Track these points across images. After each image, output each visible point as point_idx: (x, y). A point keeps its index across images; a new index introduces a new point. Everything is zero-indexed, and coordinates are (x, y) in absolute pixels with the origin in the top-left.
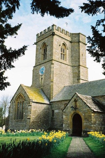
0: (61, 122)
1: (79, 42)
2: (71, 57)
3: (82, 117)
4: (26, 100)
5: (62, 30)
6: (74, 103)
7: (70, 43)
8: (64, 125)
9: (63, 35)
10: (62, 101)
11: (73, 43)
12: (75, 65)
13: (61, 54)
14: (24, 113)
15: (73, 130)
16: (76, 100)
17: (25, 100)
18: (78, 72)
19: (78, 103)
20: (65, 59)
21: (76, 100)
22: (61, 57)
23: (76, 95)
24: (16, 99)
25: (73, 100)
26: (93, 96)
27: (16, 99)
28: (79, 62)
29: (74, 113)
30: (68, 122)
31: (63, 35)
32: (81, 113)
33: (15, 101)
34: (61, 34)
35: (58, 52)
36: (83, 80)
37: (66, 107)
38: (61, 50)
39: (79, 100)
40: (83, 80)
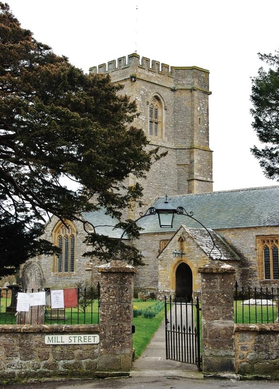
0: (151, 277)
1: (192, 148)
2: (175, 125)
3: (194, 270)
4: (79, 233)
5: (152, 65)
6: (178, 244)
7: (171, 93)
8: (160, 283)
9: (154, 77)
10: (155, 234)
11: (177, 93)
12: (184, 146)
13: (150, 122)
14: (77, 260)
15: (176, 292)
16: (181, 239)
17: (77, 233)
18: (189, 163)
19: (184, 243)
20: (159, 133)
21: (181, 239)
22: (151, 128)
23: (182, 229)
24: (55, 225)
25: (177, 238)
26: (214, 228)
27: (55, 225)
28: (192, 138)
29: (178, 262)
30: (167, 277)
31: (154, 77)
32: (191, 263)
33: (53, 233)
34: (150, 74)
35: (143, 119)
36: (192, 323)
37: (164, 251)
38: (151, 111)
39: (188, 240)
40: (192, 323)
